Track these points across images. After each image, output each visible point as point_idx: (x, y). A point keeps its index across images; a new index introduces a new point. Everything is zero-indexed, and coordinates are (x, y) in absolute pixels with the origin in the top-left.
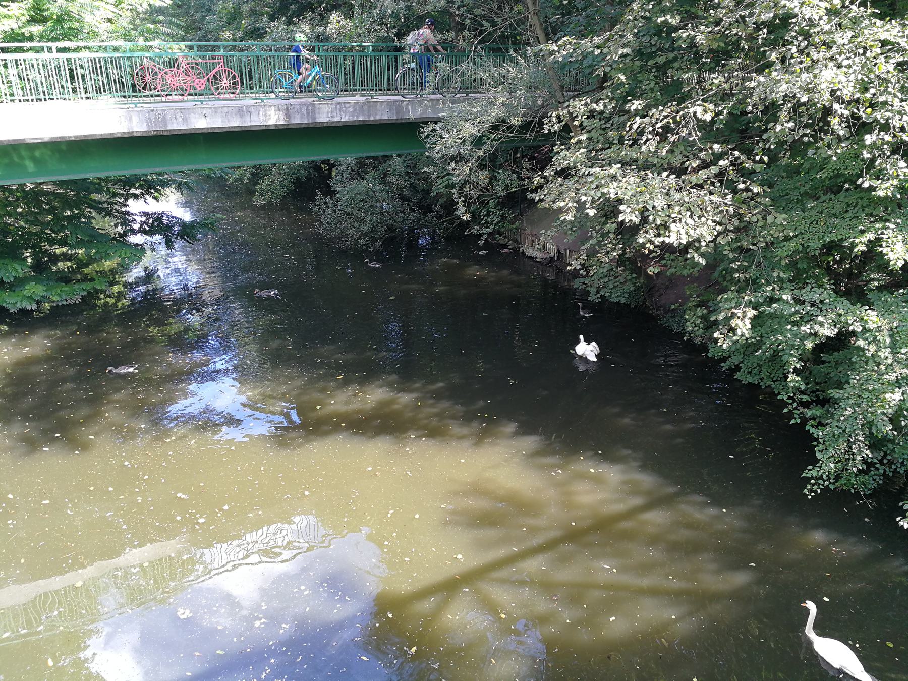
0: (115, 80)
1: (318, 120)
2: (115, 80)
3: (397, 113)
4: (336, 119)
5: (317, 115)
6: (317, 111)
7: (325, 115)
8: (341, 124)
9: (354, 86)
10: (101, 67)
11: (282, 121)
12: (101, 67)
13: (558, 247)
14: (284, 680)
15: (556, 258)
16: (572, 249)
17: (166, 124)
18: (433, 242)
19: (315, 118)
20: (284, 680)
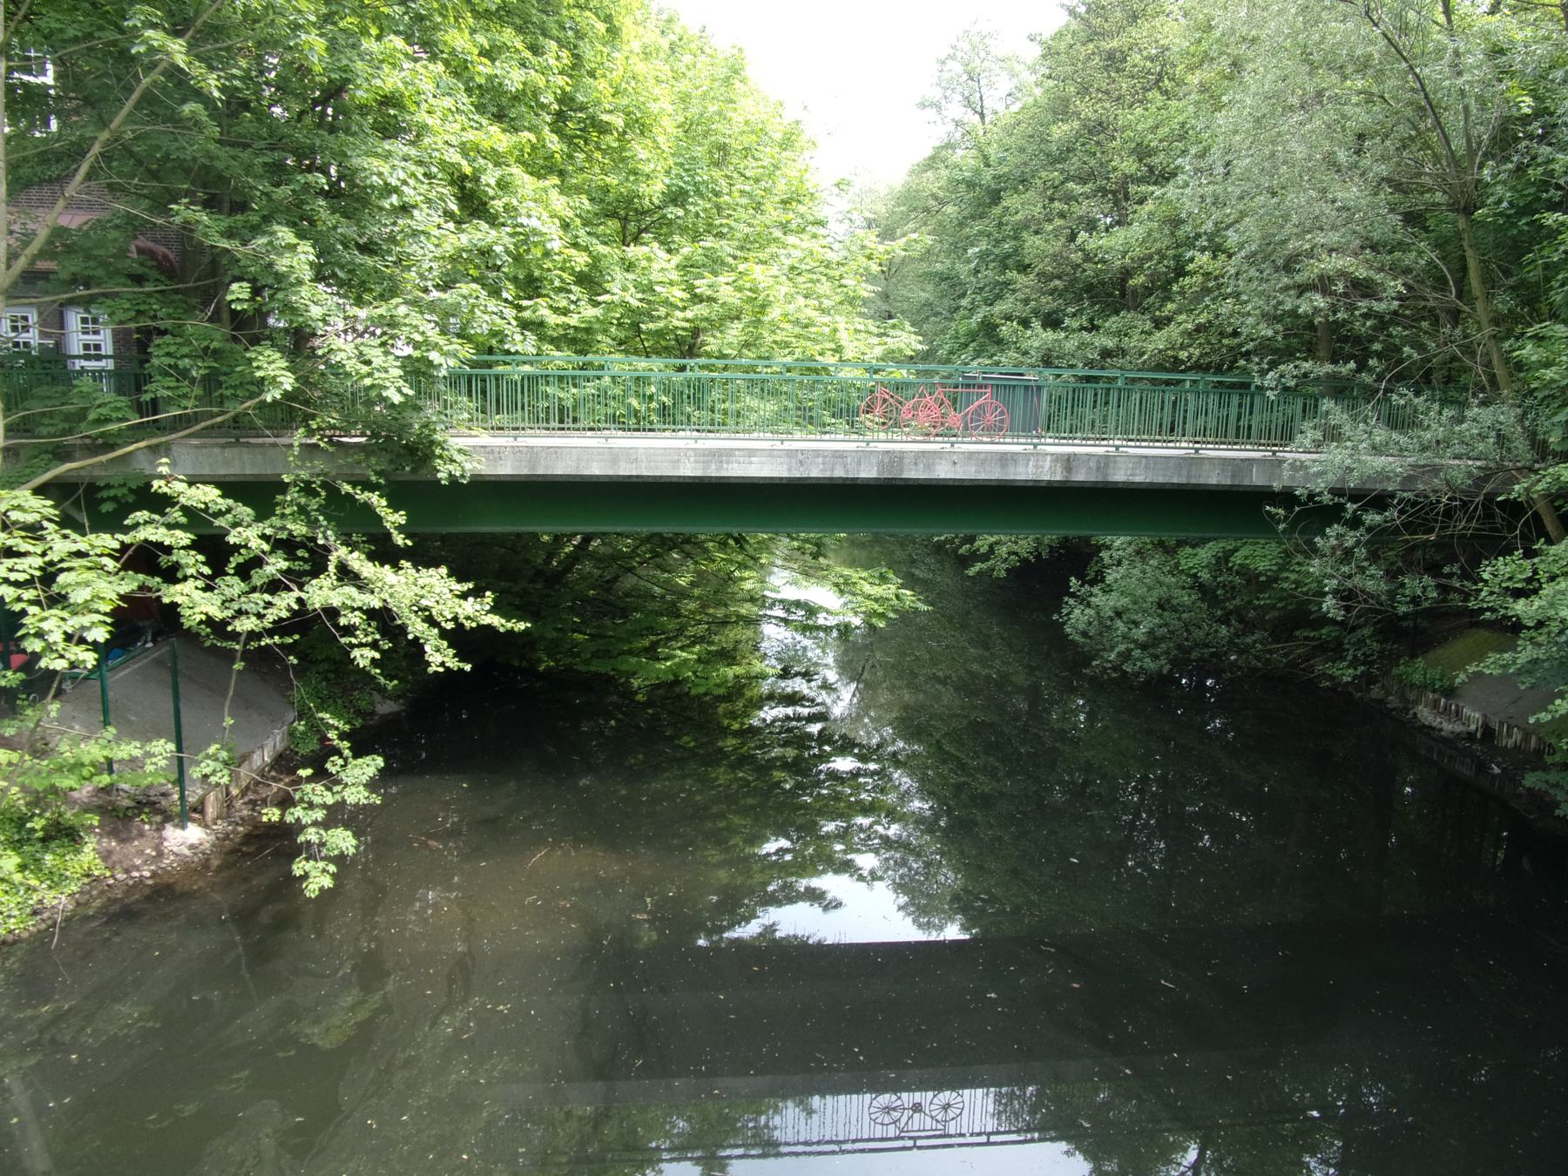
0: (523, 408)
1: (1110, 479)
2: (523, 408)
3: (1233, 476)
4: (1137, 479)
5: (1111, 471)
6: (1112, 465)
7: (1122, 472)
8: (1144, 487)
9: (1249, 437)
10: (523, 393)
11: (1058, 476)
12: (523, 393)
13: (1485, 716)
14: (1, 784)
15: (1479, 735)
16: (1513, 722)
17: (902, 471)
18: (670, 549)
19: (1107, 475)
20: (1, 784)
